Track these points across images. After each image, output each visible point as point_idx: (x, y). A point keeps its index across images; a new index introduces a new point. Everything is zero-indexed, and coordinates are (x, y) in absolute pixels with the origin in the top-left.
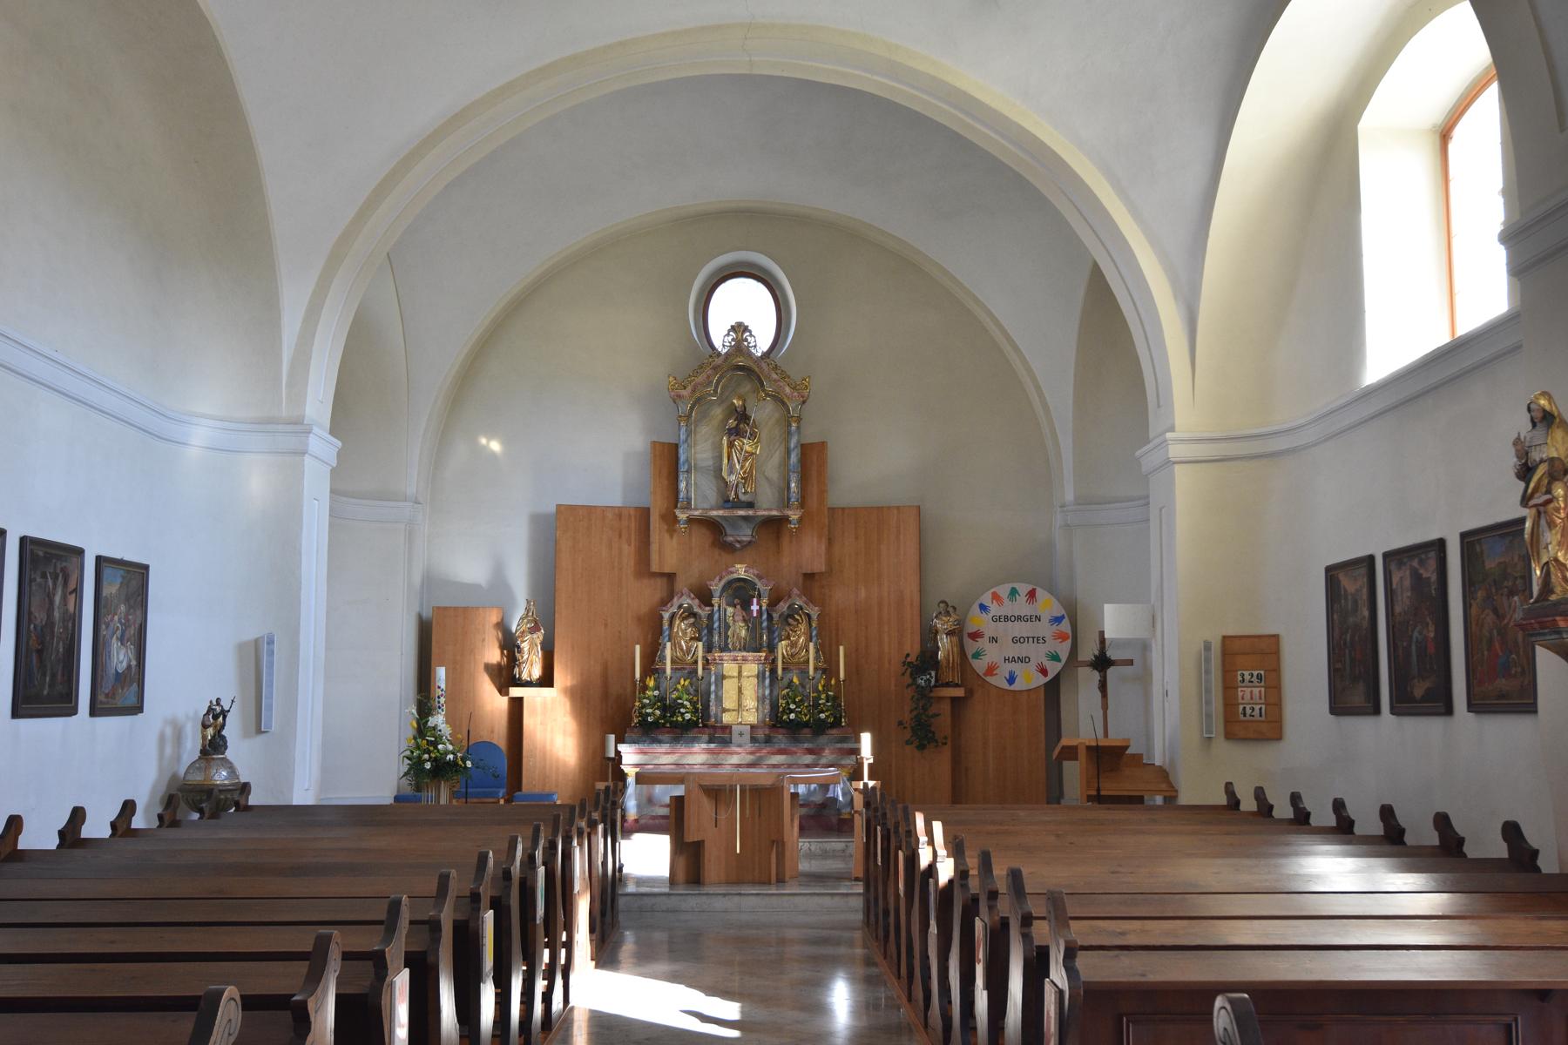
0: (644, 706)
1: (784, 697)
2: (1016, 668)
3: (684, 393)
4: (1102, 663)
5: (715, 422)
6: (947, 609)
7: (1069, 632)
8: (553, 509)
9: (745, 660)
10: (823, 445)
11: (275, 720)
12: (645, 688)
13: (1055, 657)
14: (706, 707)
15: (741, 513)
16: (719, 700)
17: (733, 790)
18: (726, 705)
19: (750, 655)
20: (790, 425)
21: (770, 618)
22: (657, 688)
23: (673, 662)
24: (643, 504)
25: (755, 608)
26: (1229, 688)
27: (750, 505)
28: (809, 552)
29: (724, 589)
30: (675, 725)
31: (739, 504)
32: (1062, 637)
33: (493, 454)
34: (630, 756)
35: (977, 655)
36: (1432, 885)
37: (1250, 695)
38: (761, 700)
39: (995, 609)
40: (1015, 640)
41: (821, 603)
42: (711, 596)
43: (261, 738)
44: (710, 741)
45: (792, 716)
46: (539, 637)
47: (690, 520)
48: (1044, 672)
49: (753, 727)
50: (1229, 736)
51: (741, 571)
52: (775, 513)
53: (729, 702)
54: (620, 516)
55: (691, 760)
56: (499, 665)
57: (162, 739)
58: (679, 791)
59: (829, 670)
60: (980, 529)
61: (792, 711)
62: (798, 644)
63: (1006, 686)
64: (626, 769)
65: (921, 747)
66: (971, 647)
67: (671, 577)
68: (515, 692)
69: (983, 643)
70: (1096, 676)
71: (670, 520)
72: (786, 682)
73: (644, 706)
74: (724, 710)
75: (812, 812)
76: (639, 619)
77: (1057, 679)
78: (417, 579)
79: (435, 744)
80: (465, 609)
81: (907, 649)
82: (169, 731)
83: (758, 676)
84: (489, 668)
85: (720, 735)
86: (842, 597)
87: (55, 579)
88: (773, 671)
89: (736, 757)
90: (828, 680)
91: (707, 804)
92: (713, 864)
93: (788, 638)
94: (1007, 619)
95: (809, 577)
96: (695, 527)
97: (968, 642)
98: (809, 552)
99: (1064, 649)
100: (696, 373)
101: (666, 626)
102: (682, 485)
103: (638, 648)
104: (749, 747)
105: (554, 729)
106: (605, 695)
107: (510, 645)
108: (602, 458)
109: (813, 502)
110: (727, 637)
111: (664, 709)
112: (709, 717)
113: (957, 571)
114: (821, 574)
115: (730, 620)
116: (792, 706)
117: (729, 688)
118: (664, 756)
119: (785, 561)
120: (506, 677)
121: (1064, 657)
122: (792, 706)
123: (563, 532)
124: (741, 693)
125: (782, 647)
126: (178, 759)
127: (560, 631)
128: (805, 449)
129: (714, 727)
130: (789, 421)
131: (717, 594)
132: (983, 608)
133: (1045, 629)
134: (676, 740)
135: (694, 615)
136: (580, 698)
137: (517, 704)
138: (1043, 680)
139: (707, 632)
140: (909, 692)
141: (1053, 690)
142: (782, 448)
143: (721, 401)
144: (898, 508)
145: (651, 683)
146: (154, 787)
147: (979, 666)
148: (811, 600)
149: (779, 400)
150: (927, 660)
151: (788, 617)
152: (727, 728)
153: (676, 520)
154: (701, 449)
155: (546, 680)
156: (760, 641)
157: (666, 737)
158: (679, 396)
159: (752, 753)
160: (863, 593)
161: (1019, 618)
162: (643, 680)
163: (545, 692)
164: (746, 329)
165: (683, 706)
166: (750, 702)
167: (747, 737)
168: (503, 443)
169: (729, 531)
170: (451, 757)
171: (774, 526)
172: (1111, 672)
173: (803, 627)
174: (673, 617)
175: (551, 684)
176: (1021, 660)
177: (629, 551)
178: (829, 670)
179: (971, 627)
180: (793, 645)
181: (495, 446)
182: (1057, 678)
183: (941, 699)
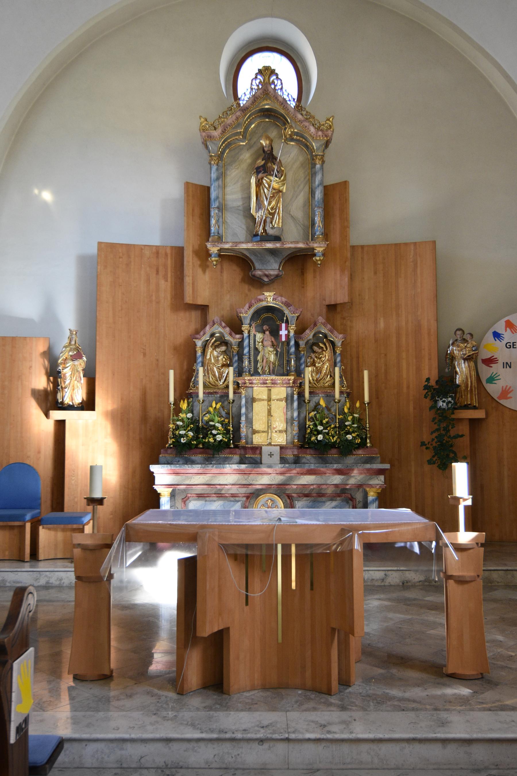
0: (178, 428)
1: (312, 419)
3: (216, 134)
5: (244, 166)
6: (462, 336)
8: (94, 250)
9: (274, 383)
10: (345, 184)
12: (178, 410)
14: (237, 428)
15: (269, 245)
16: (250, 422)
17: (271, 548)
19: (279, 379)
20: (314, 165)
21: (297, 345)
23: (205, 386)
24: (180, 244)
25: (283, 332)
27: (277, 239)
28: (331, 285)
29: (253, 318)
30: (207, 447)
31: (266, 238)
33: (45, 204)
34: (163, 476)
35: (491, 380)
36: (288, 441)
38: (290, 421)
41: (343, 331)
44: (241, 462)
45: (320, 437)
46: (81, 364)
47: (222, 256)
49: (282, 448)
51: (269, 298)
52: (301, 245)
53: (259, 424)
56: (45, 391)
59: (353, 393)
61: (319, 433)
64: (159, 489)
66: (485, 372)
67: (204, 309)
68: (57, 415)
69: (496, 369)
71: (203, 255)
72: (312, 404)
73: (178, 428)
74: (254, 432)
76: (176, 349)
80: (13, 339)
81: (426, 374)
83: (286, 399)
84: (35, 393)
86: (362, 327)
88: (301, 395)
89: (268, 476)
90: (352, 405)
91: (233, 574)
92: (243, 663)
93: (313, 364)
95: (332, 308)
96: (226, 265)
97: (482, 368)
100: (226, 114)
101: (199, 353)
103: (172, 373)
104: (279, 467)
105: (96, 450)
106: (144, 418)
107: (54, 374)
108: (145, 207)
109: (336, 238)
110: (256, 362)
111: (197, 430)
112: (240, 438)
114: (343, 304)
115: (259, 346)
116: (320, 428)
117: (259, 410)
118: (196, 475)
120: (50, 401)
122: (320, 428)
124: (270, 415)
125: (308, 373)
127: (100, 358)
128: (327, 190)
129: (245, 448)
130: (312, 162)
131: (248, 321)
132: (497, 335)
134: (208, 461)
135: (225, 343)
136: (120, 421)
137: (61, 425)
139: (237, 357)
140: (428, 415)
142: (307, 189)
144: (415, 244)
145: (184, 406)
147: (491, 388)
148: (334, 328)
149: (303, 143)
150: (445, 385)
151: (311, 346)
152: (257, 449)
154: (234, 188)
155: (89, 404)
157: (198, 457)
158: (210, 137)
159: (282, 474)
160: (382, 324)
163: (86, 414)
164: (273, 72)
165: (214, 427)
166: (279, 424)
167: (277, 458)
168: (56, 193)
169: (257, 265)
171: (299, 261)
173: (327, 355)
175: (93, 409)
177: (165, 287)
178: (353, 393)
179: (485, 354)
180: (319, 371)
181: (47, 196)
183: (460, 420)
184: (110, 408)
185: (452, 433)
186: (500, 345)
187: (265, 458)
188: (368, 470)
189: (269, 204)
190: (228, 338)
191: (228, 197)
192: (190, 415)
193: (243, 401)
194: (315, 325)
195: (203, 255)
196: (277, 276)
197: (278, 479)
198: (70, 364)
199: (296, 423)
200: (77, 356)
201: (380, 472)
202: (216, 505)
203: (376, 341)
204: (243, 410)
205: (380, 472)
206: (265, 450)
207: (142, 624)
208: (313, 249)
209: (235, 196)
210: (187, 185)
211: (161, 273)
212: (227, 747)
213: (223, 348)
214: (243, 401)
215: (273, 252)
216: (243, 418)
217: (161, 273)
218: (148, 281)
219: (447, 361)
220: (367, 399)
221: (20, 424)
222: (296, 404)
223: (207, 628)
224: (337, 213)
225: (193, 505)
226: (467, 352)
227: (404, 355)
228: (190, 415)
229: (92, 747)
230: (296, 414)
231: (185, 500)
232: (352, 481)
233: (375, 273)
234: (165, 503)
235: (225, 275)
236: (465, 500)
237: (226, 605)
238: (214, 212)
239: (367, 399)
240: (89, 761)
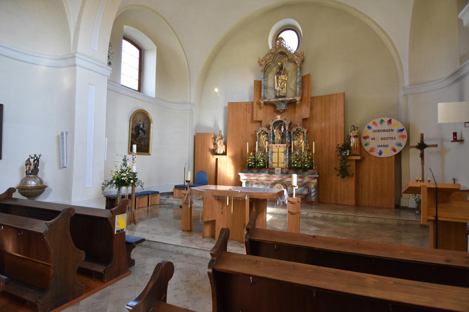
2: (382, 149)
3: (263, 63)
4: (422, 146)
6: (354, 128)
7: (406, 135)
13: (400, 145)
14: (268, 162)
15: (280, 99)
16: (272, 160)
21: (290, 133)
24: (252, 101)
25: (283, 129)
28: (304, 112)
32: (403, 137)
35: (366, 145)
38: (285, 160)
39: (374, 128)
40: (382, 139)
42: (270, 127)
45: (295, 165)
46: (222, 141)
47: (265, 104)
48: (395, 150)
53: (275, 160)
55: (261, 178)
60: (368, 100)
61: (295, 163)
62: (301, 142)
63: (378, 156)
64: (242, 181)
65: (343, 177)
66: (364, 142)
67: (261, 122)
69: (368, 140)
70: (419, 151)
71: (259, 104)
74: (273, 163)
75: (303, 197)
77: (400, 153)
78: (194, 125)
85: (271, 171)
86: (316, 126)
88: (290, 151)
89: (276, 178)
94: (379, 131)
95: (305, 120)
98: (304, 112)
99: (404, 142)
108: (241, 88)
109: (306, 95)
111: (255, 162)
113: (359, 116)
116: (296, 162)
117: (275, 155)
118: (253, 177)
119: (297, 115)
121: (404, 145)
124: (278, 155)
127: (228, 139)
131: (272, 126)
132: (369, 127)
133: (395, 134)
135: (267, 133)
136: (235, 159)
137: (217, 159)
138: (394, 153)
140: (339, 157)
141: (398, 157)
145: (251, 154)
147: (367, 148)
148: (304, 126)
150: (347, 146)
152: (273, 169)
155: (225, 154)
157: (255, 171)
160: (323, 125)
161: (384, 131)
162: (249, 153)
163: (224, 157)
165: (260, 161)
167: (280, 172)
168: (219, 89)
169: (278, 106)
171: (292, 103)
172: (426, 150)
173: (302, 136)
174: (259, 135)
176: (384, 146)
177: (249, 115)
178: (310, 150)
181: (216, 90)
182: (400, 153)
184: (231, 155)
185: (347, 165)
186: (370, 131)
187: (276, 172)
188: (311, 177)
189: (281, 85)
190: (267, 131)
191: (269, 84)
192: (253, 157)
193: (270, 153)
194: (297, 126)
195: (259, 104)
196: (285, 109)
197: (280, 179)
198: (219, 141)
199: (287, 160)
200: (222, 139)
201: (315, 178)
202: (262, 187)
203: (321, 131)
204: (270, 156)
205: (315, 178)
206: (276, 169)
208: (296, 100)
209: (270, 83)
210: (255, 81)
211: (248, 111)
212: (202, 252)
213: (266, 135)
214: (270, 153)
215: (282, 101)
216: (270, 158)
217: (248, 111)
218: (243, 114)
219: (348, 138)
220: (314, 152)
221: (208, 160)
222: (287, 154)
224: (306, 85)
225: (254, 186)
226: (355, 134)
227: (331, 136)
228: (253, 157)
229: (170, 246)
230: (287, 157)
231: (252, 185)
232: (305, 181)
233: (321, 106)
234: (244, 185)
235: (268, 110)
236: (295, 187)
238: (263, 89)
239: (314, 152)
240: (170, 250)
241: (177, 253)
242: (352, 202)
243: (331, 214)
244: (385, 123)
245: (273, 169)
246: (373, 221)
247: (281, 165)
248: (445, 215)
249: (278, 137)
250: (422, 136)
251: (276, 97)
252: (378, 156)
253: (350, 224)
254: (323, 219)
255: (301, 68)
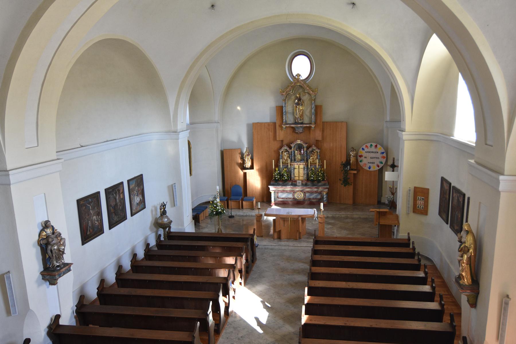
5: (293, 100)
6: (353, 149)
11: (178, 203)
12: (275, 170)
13: (381, 163)
14: (291, 175)
16: (294, 174)
18: (296, 175)
22: (279, 170)
25: (302, 152)
26: (415, 200)
27: (302, 123)
32: (384, 157)
33: (238, 110)
34: (272, 188)
35: (361, 161)
37: (420, 203)
38: (304, 174)
40: (371, 158)
43: (174, 208)
46: (249, 157)
48: (378, 166)
50: (414, 212)
53: (296, 174)
54: (269, 125)
57: (152, 211)
58: (275, 218)
59: (322, 166)
60: (364, 126)
63: (368, 169)
66: (359, 159)
68: (245, 171)
69: (362, 158)
71: (281, 126)
76: (275, 151)
79: (216, 207)
82: (153, 209)
86: (326, 145)
87: (116, 193)
88: (308, 166)
89: (298, 189)
91: (282, 222)
94: (369, 152)
97: (359, 158)
98: (318, 135)
99: (384, 161)
100: (287, 88)
102: (284, 118)
105: (255, 180)
106: (267, 170)
107: (242, 158)
108: (261, 108)
109: (318, 121)
111: (280, 176)
113: (358, 137)
117: (296, 171)
121: (384, 163)
123: (255, 129)
124: (299, 170)
126: (157, 214)
132: (363, 149)
133: (379, 155)
137: (245, 174)
138: (378, 168)
143: (294, 94)
146: (151, 222)
150: (348, 162)
152: (296, 181)
153: (282, 127)
154: (289, 108)
155: (252, 168)
156: (305, 159)
160: (331, 145)
161: (372, 152)
164: (300, 75)
167: (301, 184)
168: (241, 107)
170: (220, 210)
175: (253, 169)
176: (372, 163)
177: (271, 134)
178: (322, 166)
179: (360, 154)
181: (239, 108)
182: (382, 167)
186: (364, 152)
197: (301, 189)
200: (248, 155)
201: (327, 188)
205: (327, 188)
207: (268, 226)
219: (348, 156)
221: (237, 173)
223: (277, 230)
237: (281, 226)
241: (265, 249)
242: (351, 202)
243: (338, 214)
244: (373, 147)
245: (296, 181)
246: (362, 217)
247: (301, 178)
248: (383, 222)
249: (298, 157)
250: (394, 159)
251: (296, 123)
252: (368, 169)
253: (349, 220)
254: (333, 218)
255: (314, 100)
